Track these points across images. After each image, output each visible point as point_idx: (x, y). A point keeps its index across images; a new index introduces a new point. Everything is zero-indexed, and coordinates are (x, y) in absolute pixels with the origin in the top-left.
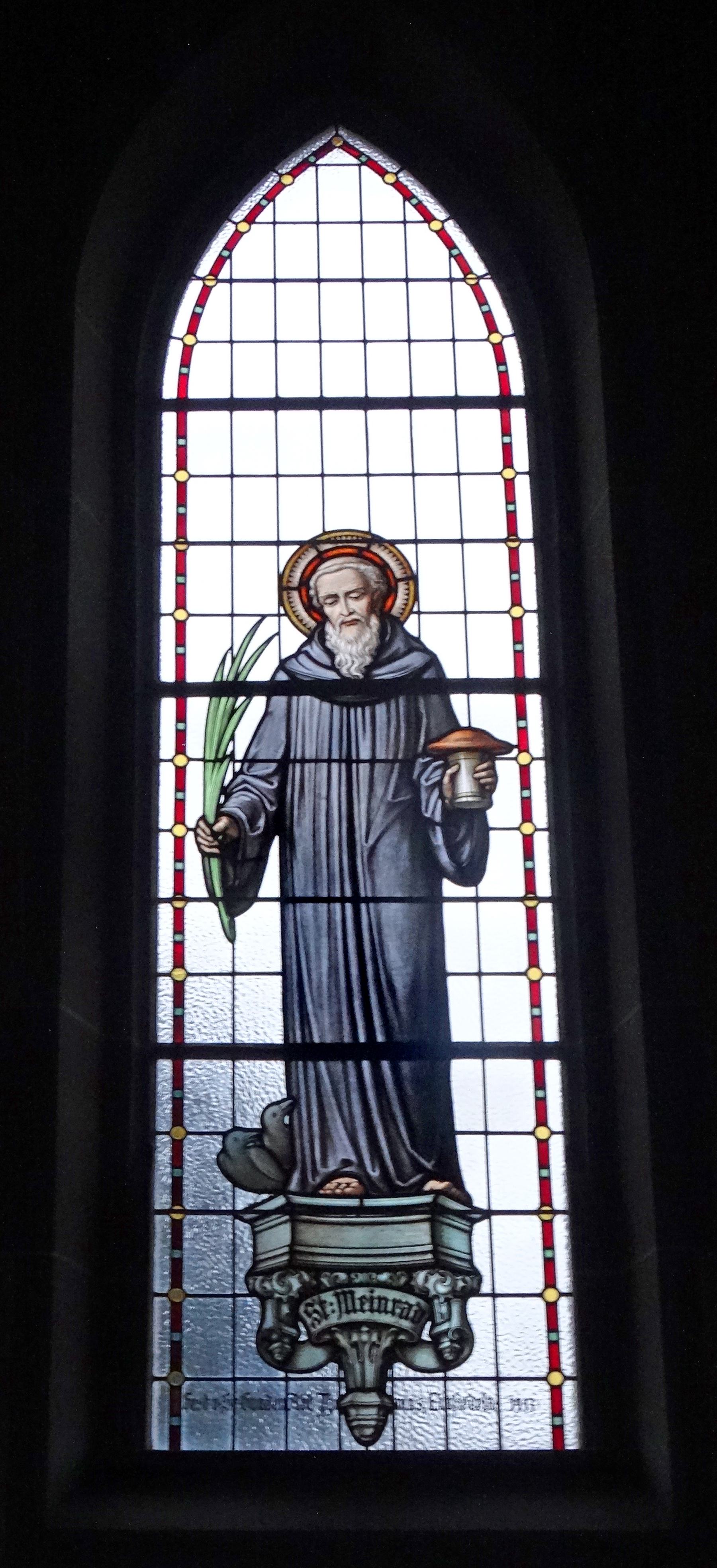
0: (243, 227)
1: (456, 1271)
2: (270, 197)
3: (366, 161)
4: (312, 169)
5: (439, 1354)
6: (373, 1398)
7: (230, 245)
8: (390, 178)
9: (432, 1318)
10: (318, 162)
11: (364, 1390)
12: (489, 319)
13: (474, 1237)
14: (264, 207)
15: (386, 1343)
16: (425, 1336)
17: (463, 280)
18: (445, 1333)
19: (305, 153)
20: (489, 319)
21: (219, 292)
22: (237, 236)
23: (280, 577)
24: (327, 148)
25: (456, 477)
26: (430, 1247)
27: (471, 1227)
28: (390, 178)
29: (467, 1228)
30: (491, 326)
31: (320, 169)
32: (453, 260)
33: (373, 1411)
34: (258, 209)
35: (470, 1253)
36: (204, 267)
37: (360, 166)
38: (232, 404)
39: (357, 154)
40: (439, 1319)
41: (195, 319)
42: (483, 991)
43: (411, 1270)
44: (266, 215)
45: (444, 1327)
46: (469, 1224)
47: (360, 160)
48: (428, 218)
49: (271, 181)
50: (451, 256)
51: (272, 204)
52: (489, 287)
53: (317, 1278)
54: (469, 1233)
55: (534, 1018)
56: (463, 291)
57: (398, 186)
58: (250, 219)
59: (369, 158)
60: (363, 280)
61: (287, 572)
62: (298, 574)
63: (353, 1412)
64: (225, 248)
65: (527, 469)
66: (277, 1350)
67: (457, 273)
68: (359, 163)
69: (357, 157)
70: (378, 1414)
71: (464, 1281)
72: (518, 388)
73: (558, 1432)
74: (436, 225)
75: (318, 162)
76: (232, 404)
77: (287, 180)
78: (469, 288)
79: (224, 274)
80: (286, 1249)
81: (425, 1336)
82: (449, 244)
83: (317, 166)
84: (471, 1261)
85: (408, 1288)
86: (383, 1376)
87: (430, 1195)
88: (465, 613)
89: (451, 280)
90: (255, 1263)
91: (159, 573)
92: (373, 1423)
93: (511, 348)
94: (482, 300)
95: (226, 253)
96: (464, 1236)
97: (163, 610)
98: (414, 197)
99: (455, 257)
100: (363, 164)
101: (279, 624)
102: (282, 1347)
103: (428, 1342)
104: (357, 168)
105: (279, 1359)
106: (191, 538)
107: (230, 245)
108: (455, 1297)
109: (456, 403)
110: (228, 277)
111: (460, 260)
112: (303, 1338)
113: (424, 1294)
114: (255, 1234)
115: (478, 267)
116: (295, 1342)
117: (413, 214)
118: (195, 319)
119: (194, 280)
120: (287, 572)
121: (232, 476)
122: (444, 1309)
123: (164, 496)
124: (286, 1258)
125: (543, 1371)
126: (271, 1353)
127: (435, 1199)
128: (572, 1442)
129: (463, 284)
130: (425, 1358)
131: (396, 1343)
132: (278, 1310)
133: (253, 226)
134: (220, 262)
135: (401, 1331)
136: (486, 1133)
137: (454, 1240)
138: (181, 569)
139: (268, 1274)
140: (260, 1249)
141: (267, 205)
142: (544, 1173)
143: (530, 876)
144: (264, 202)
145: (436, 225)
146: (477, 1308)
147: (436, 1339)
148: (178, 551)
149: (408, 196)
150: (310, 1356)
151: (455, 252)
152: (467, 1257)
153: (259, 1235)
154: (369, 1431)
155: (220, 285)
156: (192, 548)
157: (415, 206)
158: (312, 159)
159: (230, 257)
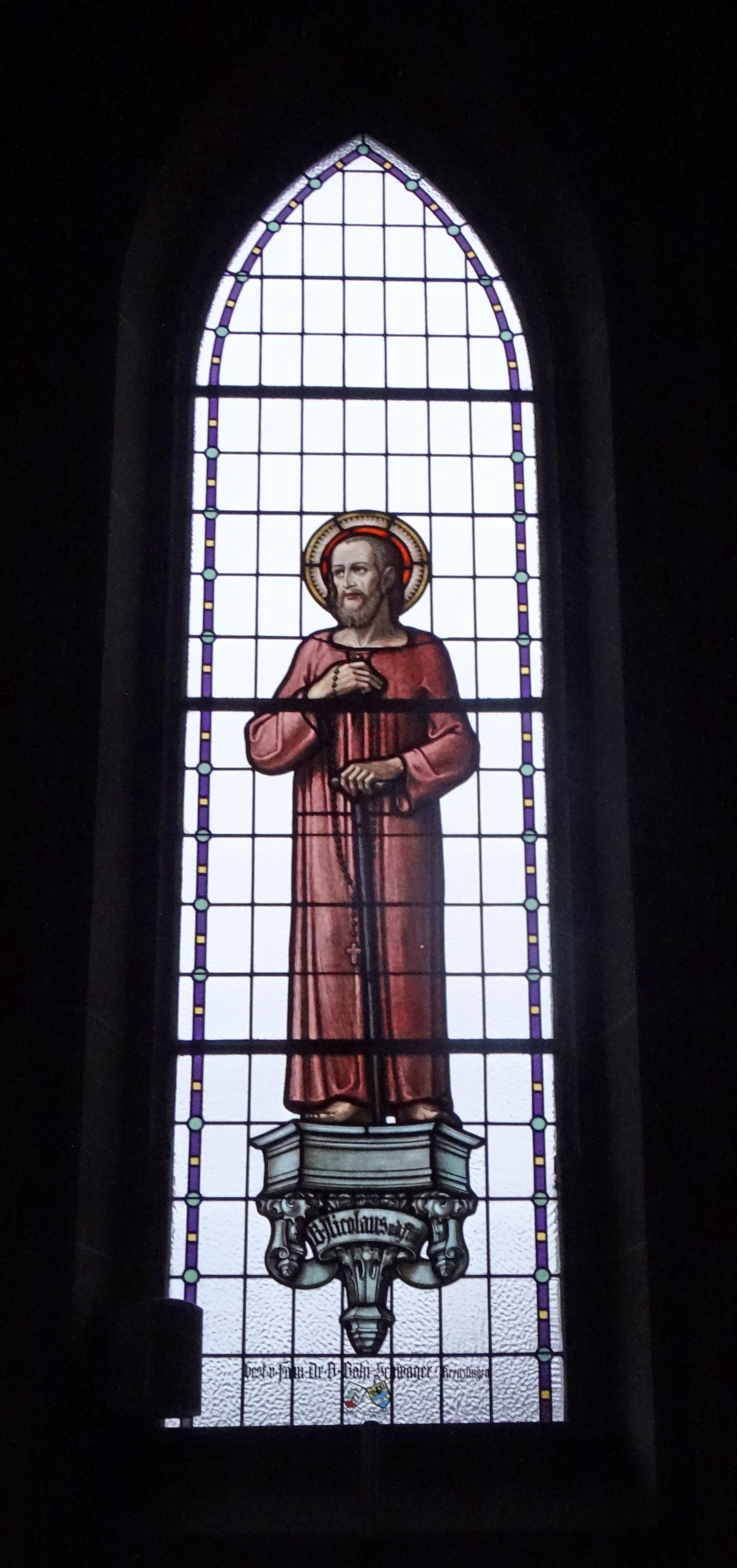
0: (274, 227)
1: (456, 1195)
2: (300, 200)
3: (391, 169)
4: (339, 175)
5: (436, 1271)
6: (374, 1313)
7: (261, 244)
8: (412, 185)
9: (429, 1237)
10: (346, 168)
11: (365, 1304)
12: (500, 316)
13: (471, 1161)
14: (292, 209)
15: (387, 1257)
16: (424, 1255)
17: (478, 281)
18: (443, 1251)
19: (333, 159)
20: (500, 316)
21: (251, 287)
22: (269, 234)
23: (303, 554)
24: (356, 154)
25: (477, 840)
26: (429, 1172)
27: (468, 1153)
28: (412, 185)
29: (465, 1155)
30: (504, 327)
31: (347, 174)
32: (468, 262)
33: (373, 1327)
34: (289, 209)
35: (467, 1177)
36: (236, 265)
37: (383, 173)
38: (260, 392)
39: (381, 161)
40: (436, 1238)
41: (228, 311)
42: (473, 441)
43: (411, 1193)
44: (295, 216)
45: (441, 1246)
46: (466, 1150)
47: (384, 168)
48: (447, 224)
49: (300, 184)
50: (467, 258)
51: (300, 206)
52: (500, 287)
53: (325, 1199)
54: (467, 1159)
55: (524, 742)
56: (476, 289)
57: (418, 192)
58: (280, 220)
59: (393, 166)
60: (384, 279)
61: (310, 550)
62: (321, 549)
63: (355, 1326)
64: (256, 246)
65: (538, 575)
66: (286, 1268)
67: (472, 274)
68: (382, 169)
69: (382, 165)
70: (378, 1328)
71: (461, 1203)
72: (526, 383)
73: (546, 1406)
74: (454, 230)
75: (346, 168)
76: (260, 392)
77: (315, 183)
78: (482, 289)
79: (255, 270)
80: (296, 1173)
81: (424, 1255)
82: (466, 247)
83: (343, 172)
84: (468, 1185)
85: (410, 1211)
86: (385, 1286)
87: (430, 1124)
88: (476, 639)
89: (466, 280)
90: (266, 1185)
91: (185, 729)
92: (373, 1336)
93: (520, 344)
94: (494, 300)
95: (257, 251)
96: (463, 1162)
97: (178, 1118)
98: (434, 202)
99: (470, 260)
100: (387, 171)
101: (303, 216)
102: (289, 1265)
103: (427, 1260)
104: (381, 175)
105: (288, 1275)
106: (220, 506)
107: (261, 244)
108: (453, 1218)
109: (469, 395)
110: (259, 274)
111: (475, 262)
112: (310, 1255)
113: (423, 1216)
114: (267, 1159)
115: (492, 270)
116: (302, 1260)
117: (432, 219)
118: (228, 311)
119: (226, 275)
120: (310, 550)
121: (252, 974)
122: (441, 1228)
123: (194, 555)
124: (295, 1181)
125: (528, 1117)
126: (280, 1270)
127: (435, 1127)
128: (558, 1415)
129: (477, 284)
130: (423, 1274)
131: (395, 1260)
132: (287, 1230)
133: (283, 226)
134: (253, 257)
135: (401, 1249)
136: (473, 515)
137: (452, 1164)
138: (202, 860)
139: (278, 1196)
140: (270, 1174)
141: (296, 207)
142: (521, 547)
143: (519, 496)
144: (293, 204)
145: (454, 230)
146: (473, 1226)
147: (433, 1258)
148: (207, 519)
149: (427, 202)
150: (315, 1273)
151: (471, 255)
152: (465, 1181)
153: (273, 1160)
154: (369, 1343)
155: (251, 281)
156: (221, 516)
157: (434, 212)
158: (340, 165)
159: (261, 255)
